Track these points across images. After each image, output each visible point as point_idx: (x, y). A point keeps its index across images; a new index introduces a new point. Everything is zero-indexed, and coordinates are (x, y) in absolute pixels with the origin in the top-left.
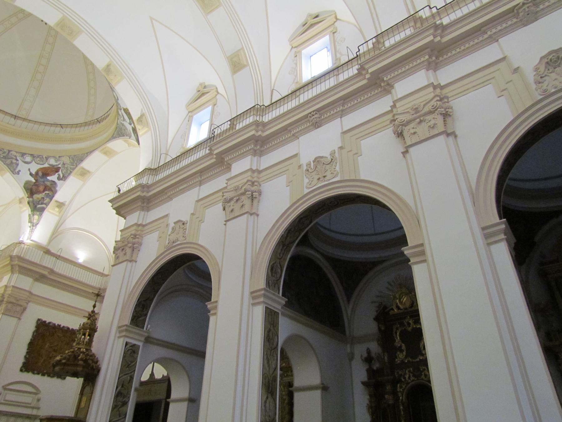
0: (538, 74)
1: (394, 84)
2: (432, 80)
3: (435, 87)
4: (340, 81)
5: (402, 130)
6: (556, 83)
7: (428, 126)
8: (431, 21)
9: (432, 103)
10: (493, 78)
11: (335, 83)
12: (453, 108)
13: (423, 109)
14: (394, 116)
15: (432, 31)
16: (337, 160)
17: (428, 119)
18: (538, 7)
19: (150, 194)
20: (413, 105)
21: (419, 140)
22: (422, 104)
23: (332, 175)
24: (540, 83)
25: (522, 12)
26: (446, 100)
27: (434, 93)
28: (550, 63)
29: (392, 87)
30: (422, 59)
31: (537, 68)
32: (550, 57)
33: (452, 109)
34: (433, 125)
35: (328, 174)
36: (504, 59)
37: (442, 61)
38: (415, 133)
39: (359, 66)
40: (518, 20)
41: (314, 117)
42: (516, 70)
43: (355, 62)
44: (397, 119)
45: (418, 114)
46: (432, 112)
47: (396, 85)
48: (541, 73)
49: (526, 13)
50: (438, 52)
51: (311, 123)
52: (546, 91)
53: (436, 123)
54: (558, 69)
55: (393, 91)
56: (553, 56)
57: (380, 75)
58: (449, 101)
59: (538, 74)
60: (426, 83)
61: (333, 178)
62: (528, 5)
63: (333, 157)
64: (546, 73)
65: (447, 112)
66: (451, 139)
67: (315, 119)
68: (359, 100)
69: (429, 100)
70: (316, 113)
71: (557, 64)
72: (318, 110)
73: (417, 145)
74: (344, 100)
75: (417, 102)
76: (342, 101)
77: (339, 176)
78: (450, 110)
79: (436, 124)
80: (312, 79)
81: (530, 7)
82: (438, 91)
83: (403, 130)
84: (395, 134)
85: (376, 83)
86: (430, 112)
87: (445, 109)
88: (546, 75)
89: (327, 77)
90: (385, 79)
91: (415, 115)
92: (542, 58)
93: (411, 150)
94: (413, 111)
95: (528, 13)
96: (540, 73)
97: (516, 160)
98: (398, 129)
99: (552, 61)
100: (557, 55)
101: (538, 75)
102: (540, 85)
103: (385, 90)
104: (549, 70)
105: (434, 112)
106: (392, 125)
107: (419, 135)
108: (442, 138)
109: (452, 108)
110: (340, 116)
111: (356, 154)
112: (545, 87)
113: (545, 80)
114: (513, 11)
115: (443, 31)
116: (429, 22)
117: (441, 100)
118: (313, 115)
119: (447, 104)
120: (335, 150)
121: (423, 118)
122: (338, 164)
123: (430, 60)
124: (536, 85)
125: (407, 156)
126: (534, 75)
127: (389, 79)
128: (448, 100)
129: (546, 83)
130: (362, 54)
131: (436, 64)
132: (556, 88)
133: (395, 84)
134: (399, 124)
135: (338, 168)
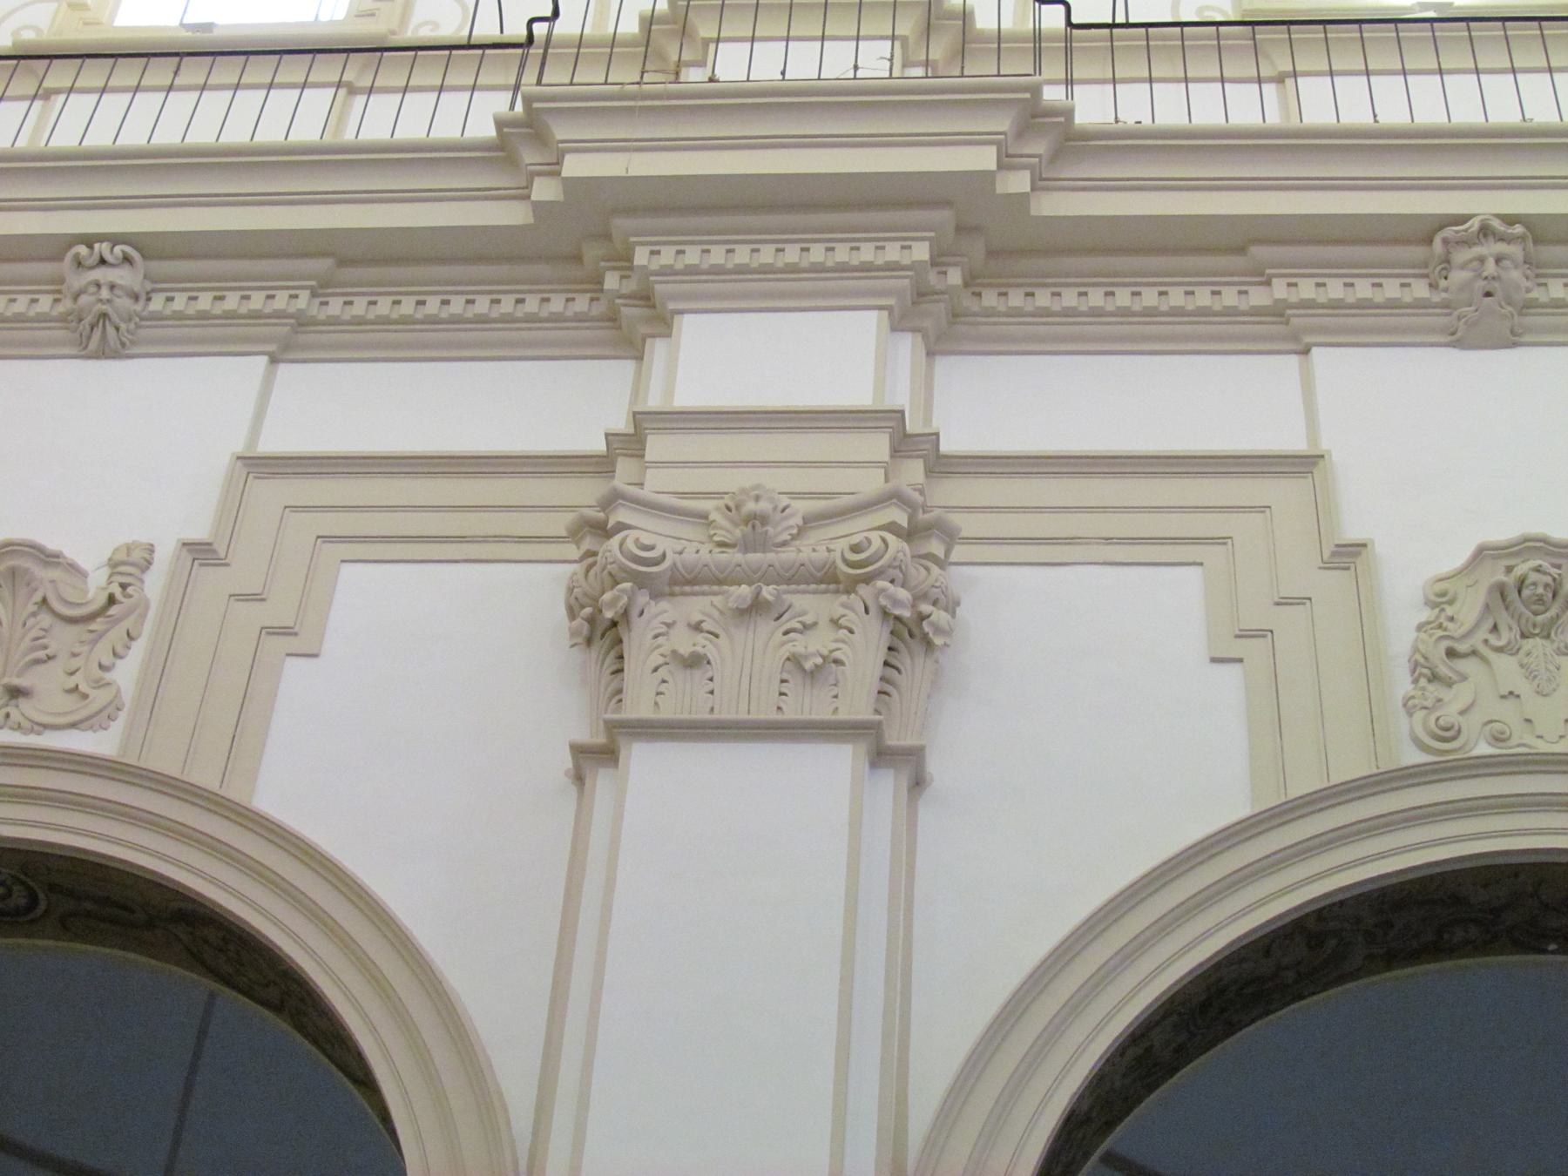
0: (1440, 626)
1: (682, 312)
2: (900, 396)
3: (904, 444)
4: (54, 143)
5: (626, 613)
6: (1508, 713)
7: (785, 652)
8: (1017, 66)
9: (857, 529)
10: (1222, 541)
11: (22, 143)
12: (959, 611)
13: (794, 537)
14: (612, 500)
15: (1002, 123)
16: (143, 616)
17: (804, 613)
18: (1540, 280)
19: (1057, 205)
20: (744, 491)
21: (703, 715)
22: (802, 507)
23: (71, 702)
24: (1434, 678)
25: (1463, 267)
26: (936, 548)
27: (887, 480)
28: (1513, 595)
29: (663, 324)
30: (893, 253)
31: (1443, 594)
32: (1522, 568)
33: (953, 614)
34: (819, 661)
35: (48, 684)
36: (1304, 464)
37: (990, 312)
38: (694, 662)
39: (519, 107)
40: (1436, 298)
41: (100, 274)
42: (1348, 555)
43: (500, 70)
44: (622, 527)
45: (754, 557)
46: (837, 581)
47: (694, 330)
48: (1454, 629)
49: (1480, 285)
50: (992, 253)
51: (66, 305)
52: (1454, 738)
53: (837, 655)
54: (1535, 645)
55: (658, 350)
56: (1538, 570)
57: (620, 224)
58: (954, 557)
59: (1440, 626)
60: (860, 396)
61: (73, 725)
62: (1501, 248)
63: (124, 586)
64: (1476, 641)
65: (923, 617)
66: (887, 786)
67: (105, 293)
68: (433, 306)
69: (845, 501)
70: (127, 259)
71: (1540, 618)
72: (147, 247)
73: (671, 737)
74: (343, 262)
75: (775, 480)
76: (322, 265)
77: (117, 727)
78: (939, 616)
79: (837, 662)
80: (185, 34)
81: (1506, 263)
82: (913, 472)
83: (635, 612)
84: (572, 614)
85: (577, 258)
86: (828, 579)
87: (920, 597)
88: (1474, 653)
89: (293, 69)
90: (641, 257)
91: (734, 556)
92: (1483, 554)
93: (641, 757)
94: (735, 524)
95: (1488, 289)
96: (1450, 625)
97: (1182, 1056)
98: (607, 596)
99: (1526, 592)
100: (1554, 571)
101: (1440, 633)
102: (1434, 690)
103: (613, 319)
104: (1495, 628)
105: (850, 586)
106: (572, 551)
107: (715, 685)
108: (842, 759)
109: (952, 607)
110: (272, 348)
111: (287, 632)
112: (1450, 714)
113: (1464, 678)
114: (1429, 241)
115: (1057, 155)
116: (647, 78)
117: (910, 534)
118: (103, 262)
119: (935, 570)
120: (151, 549)
121: (778, 596)
122: (138, 649)
123: (933, 278)
124: (1416, 681)
125: (602, 781)
126: (1420, 628)
127: (667, 271)
128: (948, 553)
129: (1456, 699)
130: (565, 43)
131: (956, 315)
132: (1498, 739)
133: (687, 317)
134: (623, 569)
135: (126, 674)
